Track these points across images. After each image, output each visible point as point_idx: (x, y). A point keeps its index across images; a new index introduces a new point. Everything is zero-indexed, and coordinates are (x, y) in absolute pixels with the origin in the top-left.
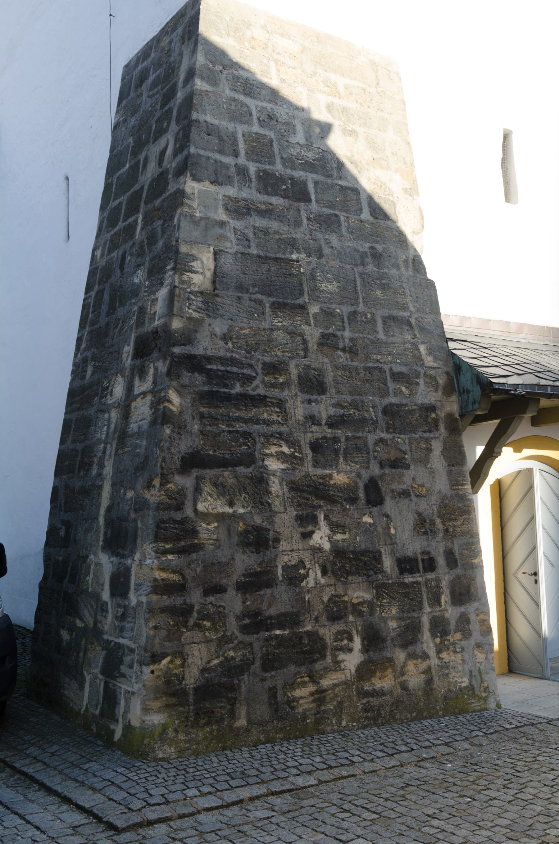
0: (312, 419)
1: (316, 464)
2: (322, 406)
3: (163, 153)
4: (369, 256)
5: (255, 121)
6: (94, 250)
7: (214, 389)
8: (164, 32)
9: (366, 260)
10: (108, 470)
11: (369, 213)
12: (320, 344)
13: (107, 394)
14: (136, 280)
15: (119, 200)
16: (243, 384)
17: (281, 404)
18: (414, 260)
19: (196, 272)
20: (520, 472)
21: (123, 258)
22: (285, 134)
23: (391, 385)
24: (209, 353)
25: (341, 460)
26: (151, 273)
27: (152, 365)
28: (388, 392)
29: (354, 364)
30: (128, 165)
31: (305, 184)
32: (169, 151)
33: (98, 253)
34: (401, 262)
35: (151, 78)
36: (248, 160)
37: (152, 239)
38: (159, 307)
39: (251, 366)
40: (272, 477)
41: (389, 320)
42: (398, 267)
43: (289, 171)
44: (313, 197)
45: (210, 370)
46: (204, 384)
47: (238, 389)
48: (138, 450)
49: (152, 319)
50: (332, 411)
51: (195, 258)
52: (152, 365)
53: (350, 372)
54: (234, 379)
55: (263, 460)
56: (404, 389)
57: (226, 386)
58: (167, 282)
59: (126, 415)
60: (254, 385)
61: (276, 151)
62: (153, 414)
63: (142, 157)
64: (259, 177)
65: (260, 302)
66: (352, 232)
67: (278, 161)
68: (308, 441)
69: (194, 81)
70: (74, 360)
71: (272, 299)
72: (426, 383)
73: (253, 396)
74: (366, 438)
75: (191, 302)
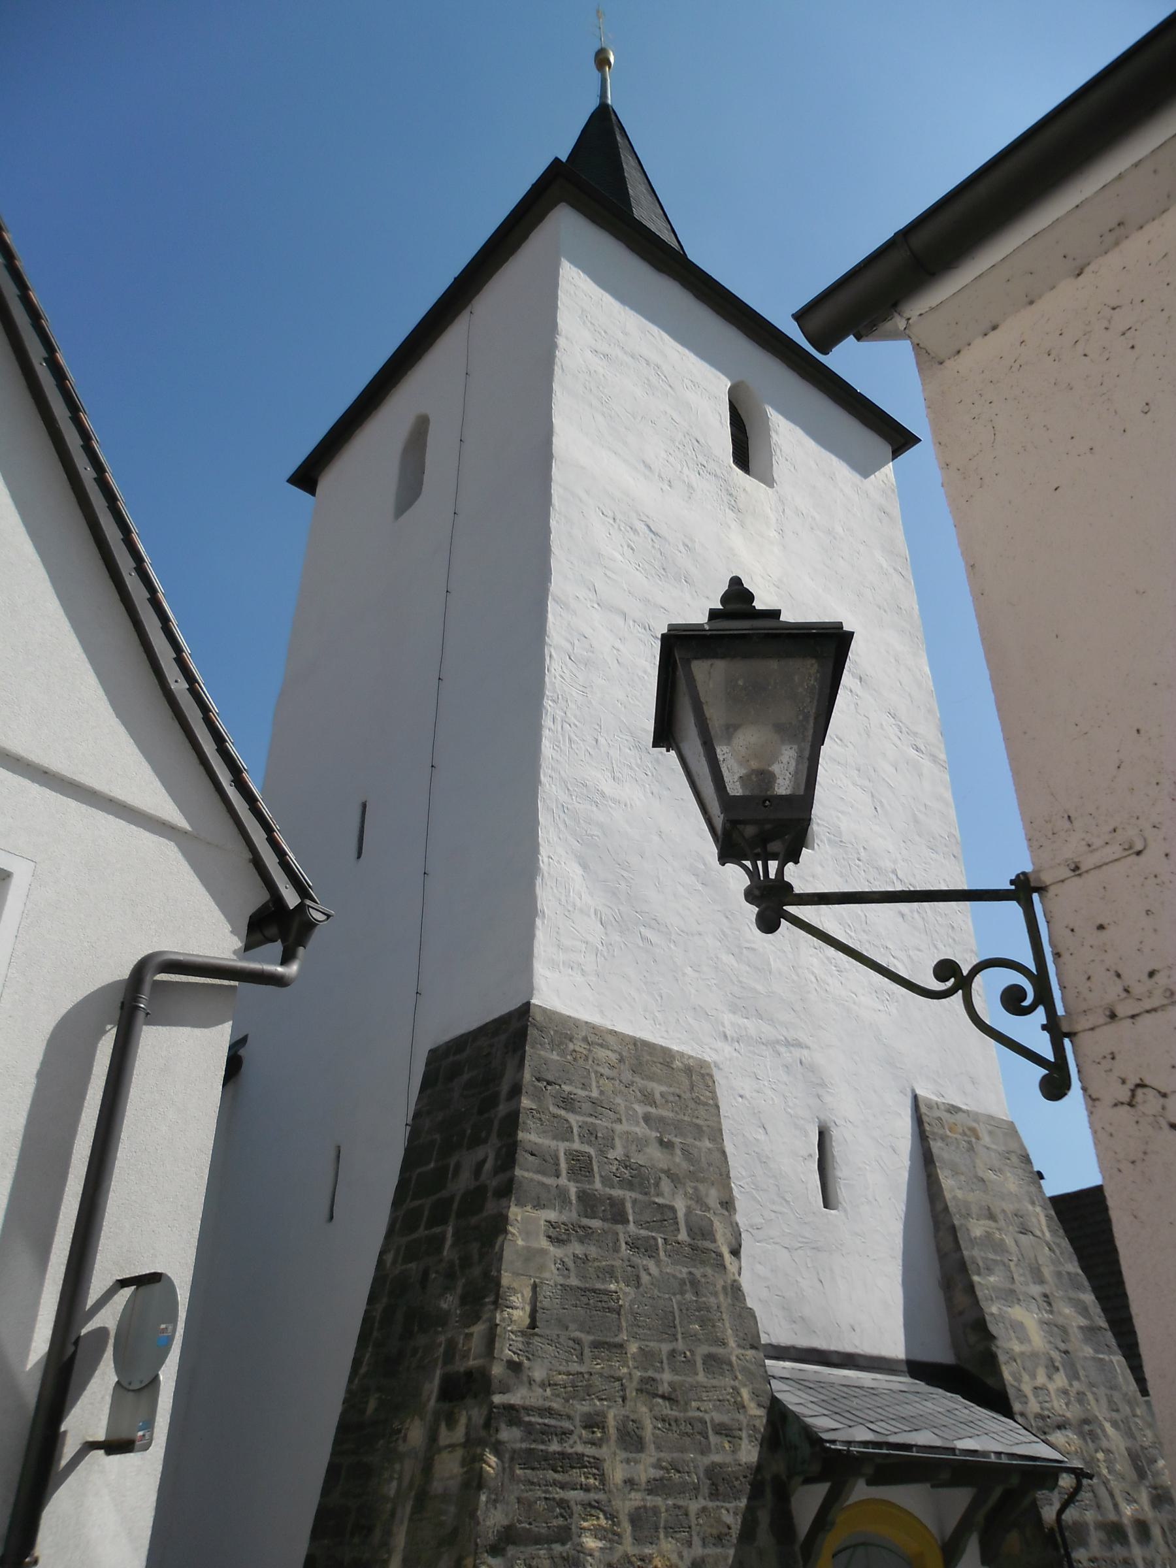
0: (630, 1483)
1: (637, 1540)
2: (641, 1467)
3: (481, 1164)
4: (688, 1283)
5: (576, 1138)
6: (382, 1254)
7: (532, 1446)
8: (482, 1031)
9: (685, 1288)
10: (400, 1539)
11: (686, 1234)
12: (640, 1391)
13: (397, 1439)
14: (444, 1306)
15: (420, 1202)
16: (561, 1442)
17: (597, 1463)
18: (733, 1285)
19: (517, 1308)
20: (740, 1246)
21: (426, 1273)
22: (604, 1149)
23: (713, 1439)
24: (527, 1403)
25: (662, 1535)
26: (464, 1300)
27: (464, 1413)
28: (710, 1448)
29: (673, 1413)
30: (432, 1165)
31: (622, 1202)
32: (488, 1166)
33: (389, 1258)
34: (719, 1287)
35: (466, 1077)
36: (569, 1181)
37: (466, 1262)
38: (476, 1344)
39: (569, 1417)
40: (589, 1558)
41: (710, 1360)
42: (715, 1294)
43: (607, 1190)
44: (631, 1218)
45: (530, 1423)
46: (522, 1440)
47: (554, 1447)
48: (444, 1518)
49: (465, 1356)
50: (654, 1473)
51: (515, 1292)
52: (464, 1413)
53: (670, 1425)
54: (552, 1434)
55: (580, 1536)
56: (727, 1445)
57: (543, 1442)
58: (485, 1316)
59: (427, 1468)
60: (571, 1442)
61: (596, 1168)
62: (466, 1473)
63: (452, 1162)
64: (579, 1198)
65: (577, 1341)
66: (670, 1256)
67: (597, 1179)
68: (626, 1512)
69: (520, 1098)
70: (347, 1386)
71: (591, 1338)
72: (750, 1436)
73: (571, 1454)
74: (687, 1507)
75: (511, 1342)
